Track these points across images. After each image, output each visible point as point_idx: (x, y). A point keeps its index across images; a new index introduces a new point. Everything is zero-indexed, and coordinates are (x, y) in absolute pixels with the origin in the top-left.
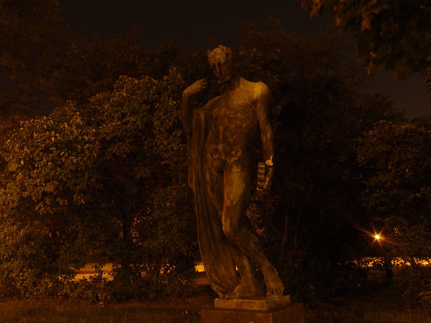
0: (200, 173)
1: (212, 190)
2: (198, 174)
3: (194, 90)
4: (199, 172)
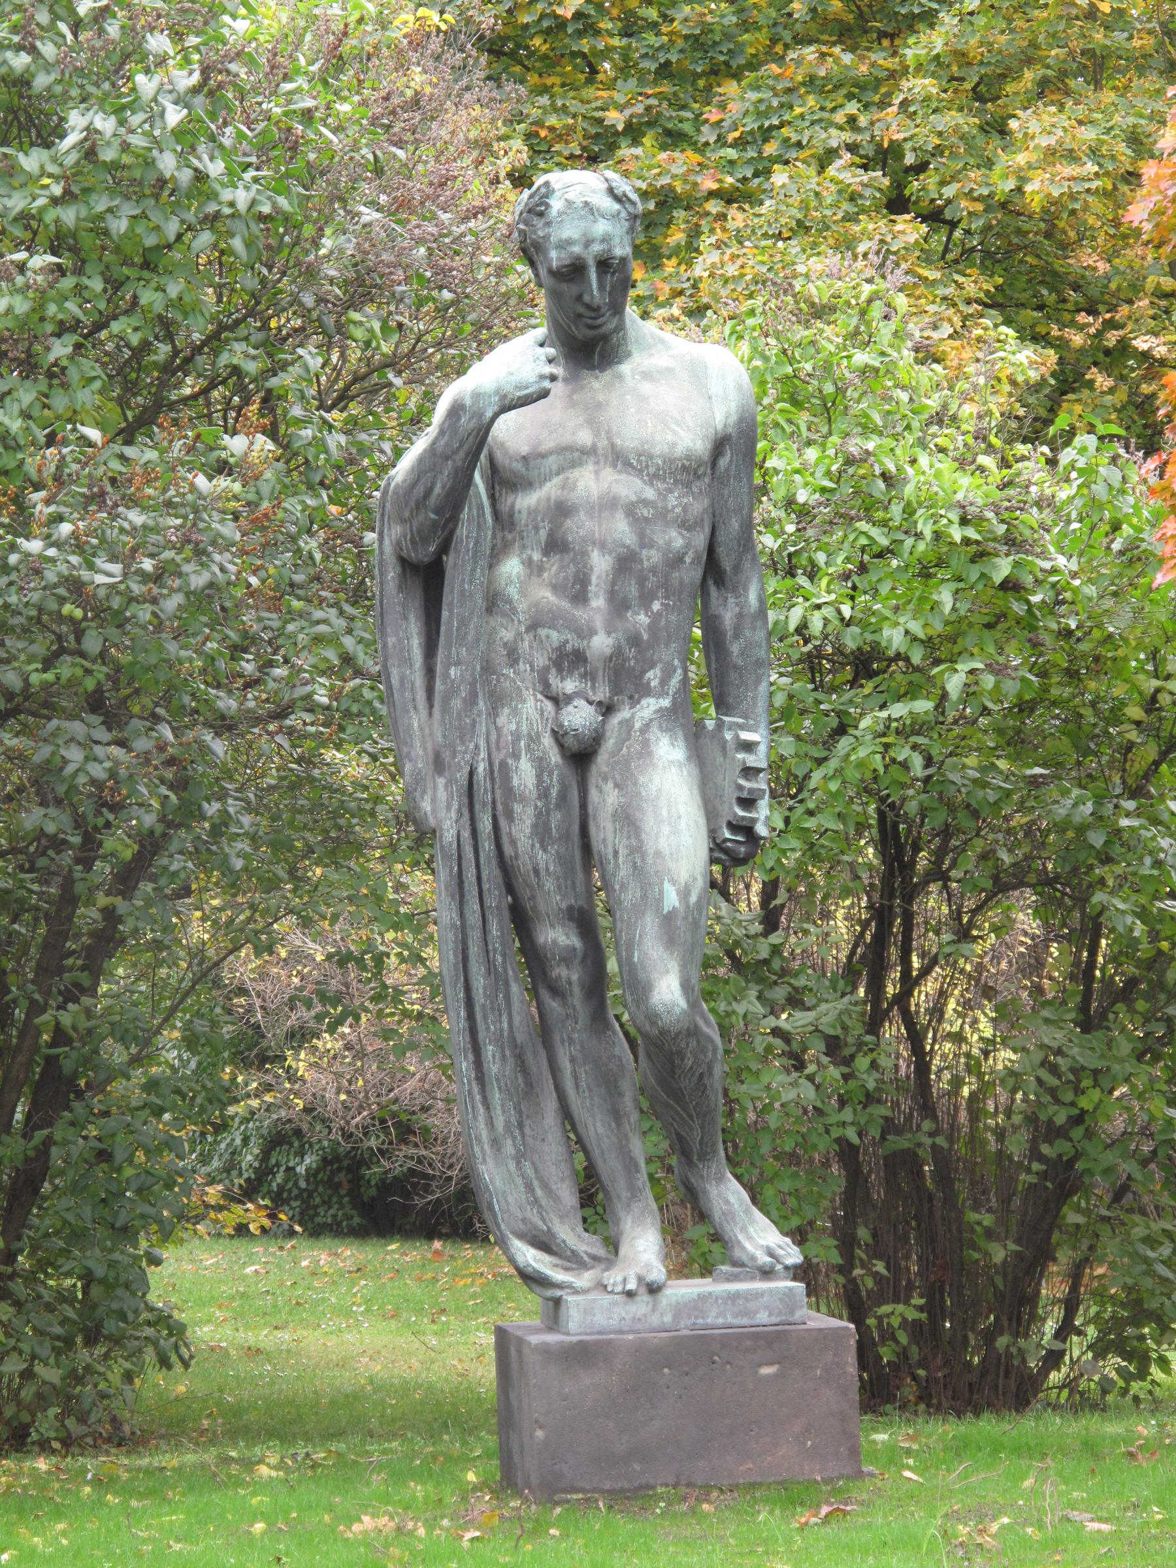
1: (541, 831)
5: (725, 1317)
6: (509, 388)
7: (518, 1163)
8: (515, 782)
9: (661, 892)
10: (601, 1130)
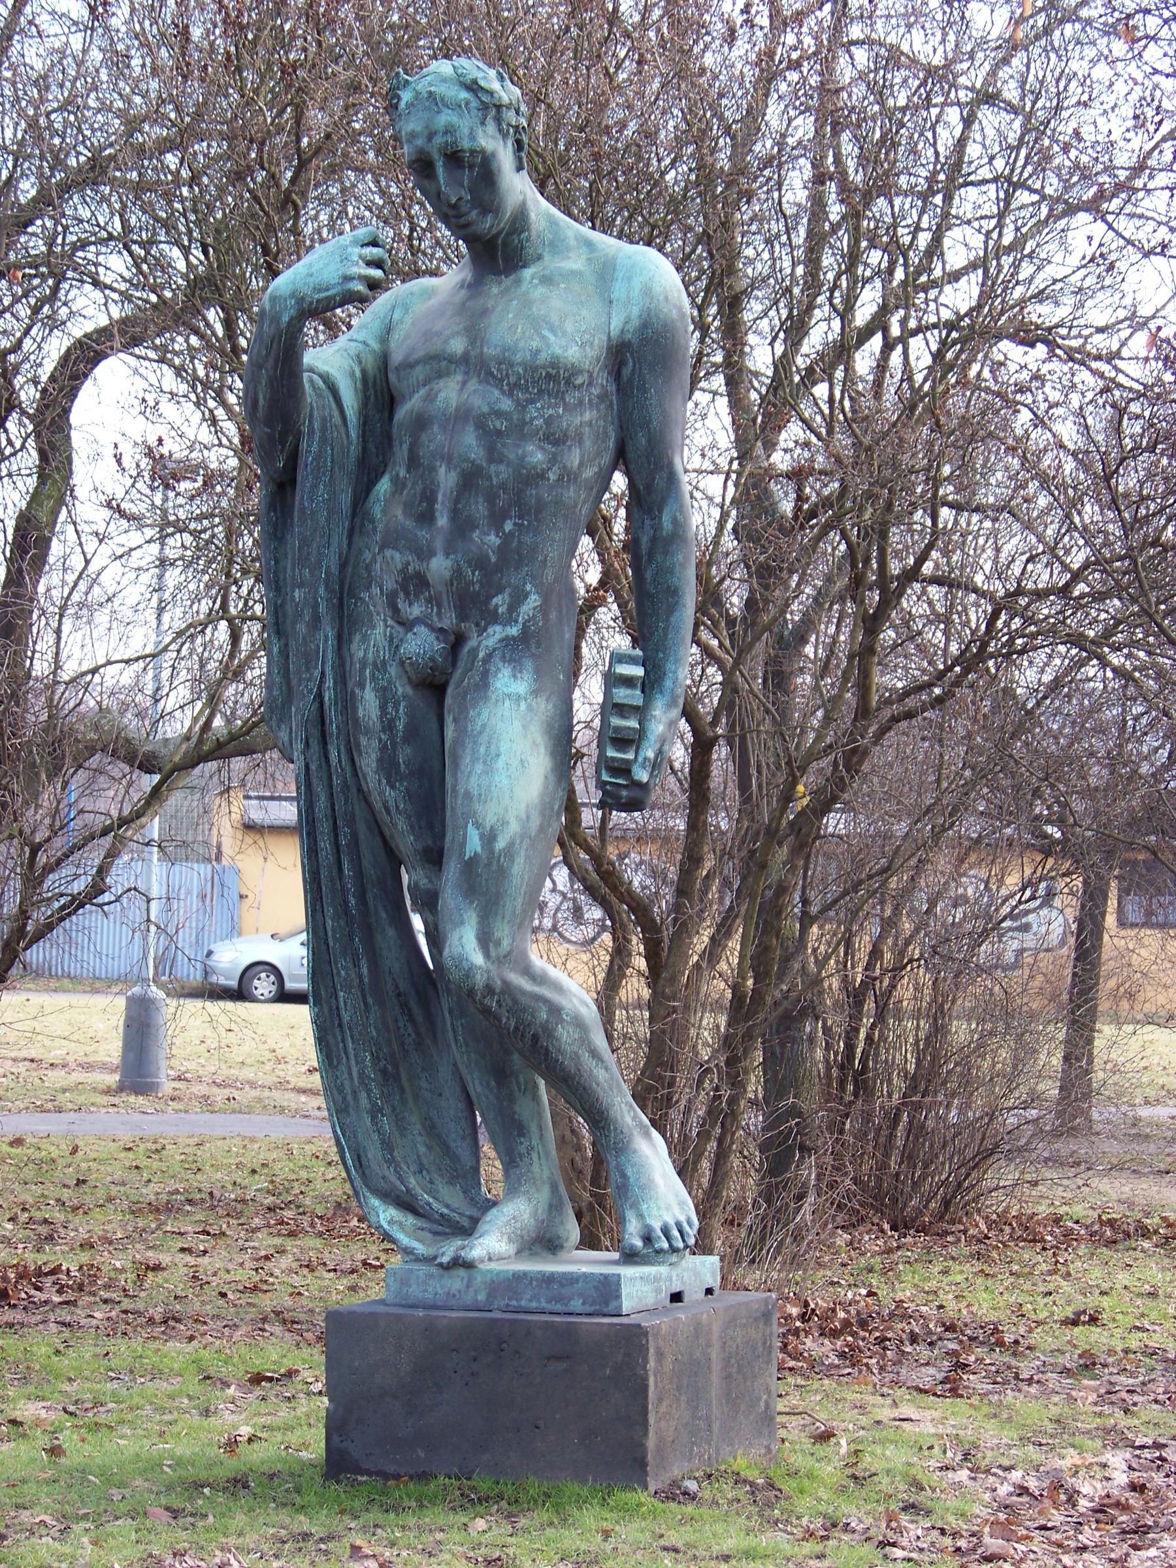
0: (329, 683)
1: (388, 766)
2: (320, 688)
3: (327, 290)
4: (323, 673)
5: (539, 1301)
6: (307, 290)
7: (374, 1118)
8: (361, 713)
9: (465, 835)
10: (479, 1089)
